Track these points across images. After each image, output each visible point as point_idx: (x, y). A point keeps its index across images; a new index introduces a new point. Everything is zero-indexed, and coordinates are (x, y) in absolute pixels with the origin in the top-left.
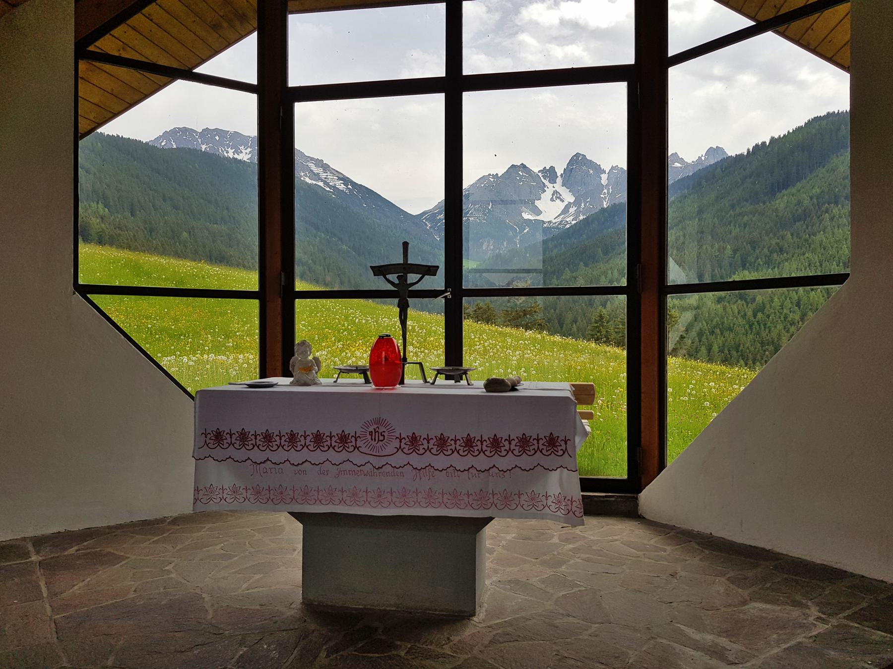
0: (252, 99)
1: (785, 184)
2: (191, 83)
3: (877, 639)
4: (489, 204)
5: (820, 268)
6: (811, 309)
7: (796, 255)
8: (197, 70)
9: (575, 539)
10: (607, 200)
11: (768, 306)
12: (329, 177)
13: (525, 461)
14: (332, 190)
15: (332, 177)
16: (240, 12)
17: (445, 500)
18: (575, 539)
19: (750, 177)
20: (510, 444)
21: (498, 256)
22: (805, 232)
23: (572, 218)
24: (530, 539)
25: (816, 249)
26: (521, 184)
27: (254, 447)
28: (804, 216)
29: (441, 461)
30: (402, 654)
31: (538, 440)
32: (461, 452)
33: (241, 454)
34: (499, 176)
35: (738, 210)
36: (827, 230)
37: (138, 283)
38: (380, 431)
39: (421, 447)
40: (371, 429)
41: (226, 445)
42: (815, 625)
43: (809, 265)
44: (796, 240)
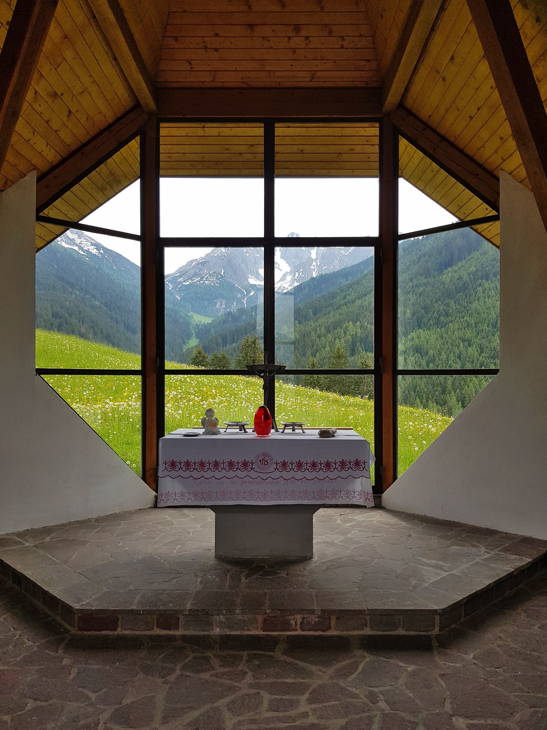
0: (137, 245)
1: (449, 263)
3: (513, 558)
4: (222, 271)
5: (475, 329)
6: (469, 361)
7: (458, 318)
9: (350, 521)
10: (316, 271)
11: (437, 359)
12: (83, 242)
13: (344, 474)
14: (86, 254)
15: (86, 243)
17: (301, 496)
18: (350, 521)
19: (424, 257)
20: (336, 465)
21: (230, 314)
22: (464, 301)
23: (289, 284)
24: (325, 522)
25: (472, 314)
26: (248, 255)
27: (194, 469)
28: (464, 288)
29: (299, 475)
30: (285, 576)
31: (350, 463)
32: (310, 470)
33: (187, 474)
35: (415, 282)
36: (480, 300)
37: (124, 378)
38: (266, 460)
39: (288, 468)
40: (261, 458)
41: (177, 469)
42: (484, 555)
43: (468, 326)
44: (458, 307)
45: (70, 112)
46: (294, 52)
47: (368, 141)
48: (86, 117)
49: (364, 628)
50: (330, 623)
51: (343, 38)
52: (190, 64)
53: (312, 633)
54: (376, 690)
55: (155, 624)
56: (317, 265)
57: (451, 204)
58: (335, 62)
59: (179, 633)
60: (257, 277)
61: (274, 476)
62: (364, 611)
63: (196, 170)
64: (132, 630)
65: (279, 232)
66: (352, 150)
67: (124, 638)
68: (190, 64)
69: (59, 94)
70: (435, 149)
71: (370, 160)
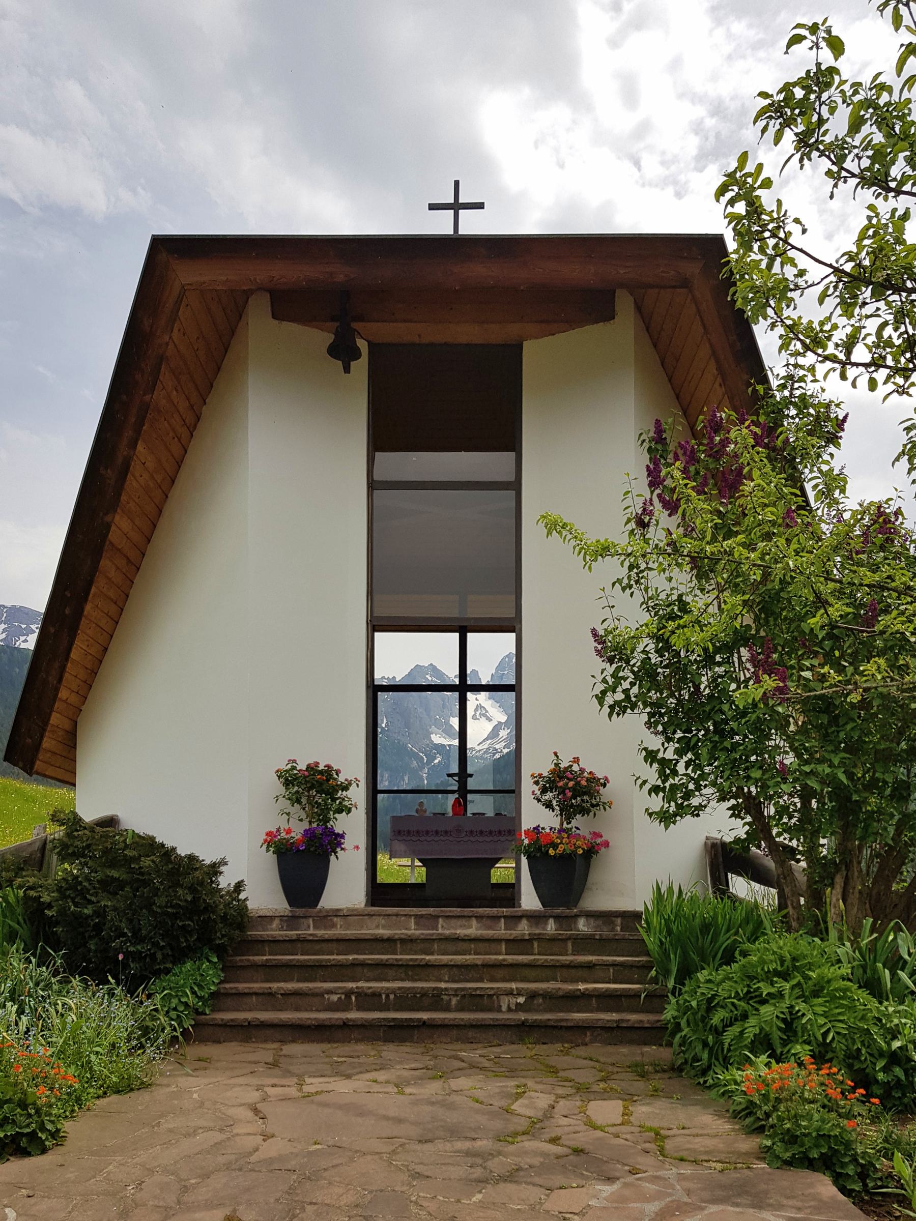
23: (503, 744)
29: (481, 839)
60: (448, 731)
61: (464, 839)
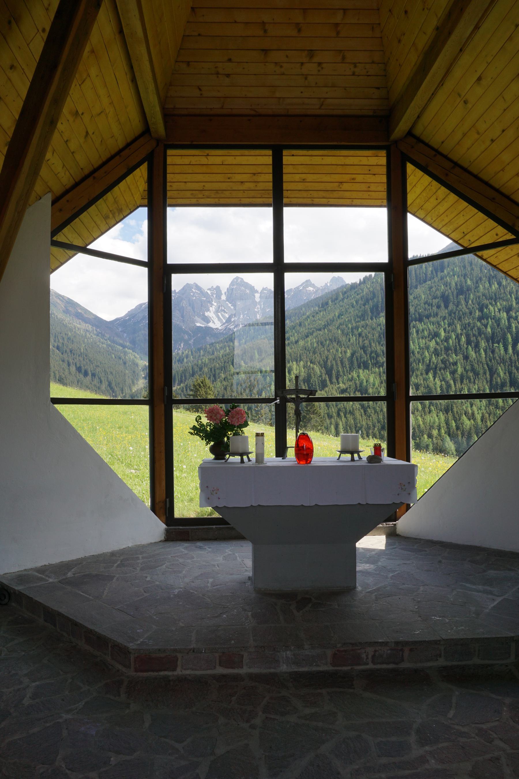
2: (111, 261)
8: (89, 247)
16: (120, 208)
26: (194, 298)
34: (177, 291)
45: (87, 133)
46: (306, 79)
47: (370, 170)
48: (101, 140)
49: (438, 658)
50: (402, 655)
51: (355, 65)
52: (200, 90)
53: (384, 666)
54: (484, 727)
55: (218, 661)
56: (261, 308)
57: (454, 232)
58: (345, 89)
59: (244, 671)
62: (439, 641)
63: (196, 199)
64: (193, 670)
65: (288, 258)
66: (354, 179)
67: (182, 680)
68: (200, 90)
69: (80, 113)
70: (447, 175)
71: (370, 189)
